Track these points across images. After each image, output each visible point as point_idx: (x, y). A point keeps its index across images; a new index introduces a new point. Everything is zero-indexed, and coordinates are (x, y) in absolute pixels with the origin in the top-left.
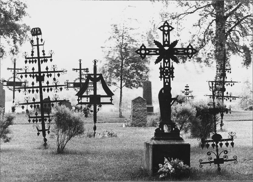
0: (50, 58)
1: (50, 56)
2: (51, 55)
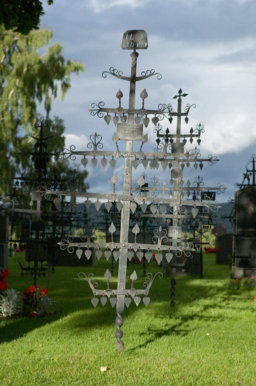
0: (197, 138)
1: (197, 133)
2: (200, 131)
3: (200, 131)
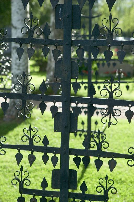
2: (106, 192)
3: (106, 192)
